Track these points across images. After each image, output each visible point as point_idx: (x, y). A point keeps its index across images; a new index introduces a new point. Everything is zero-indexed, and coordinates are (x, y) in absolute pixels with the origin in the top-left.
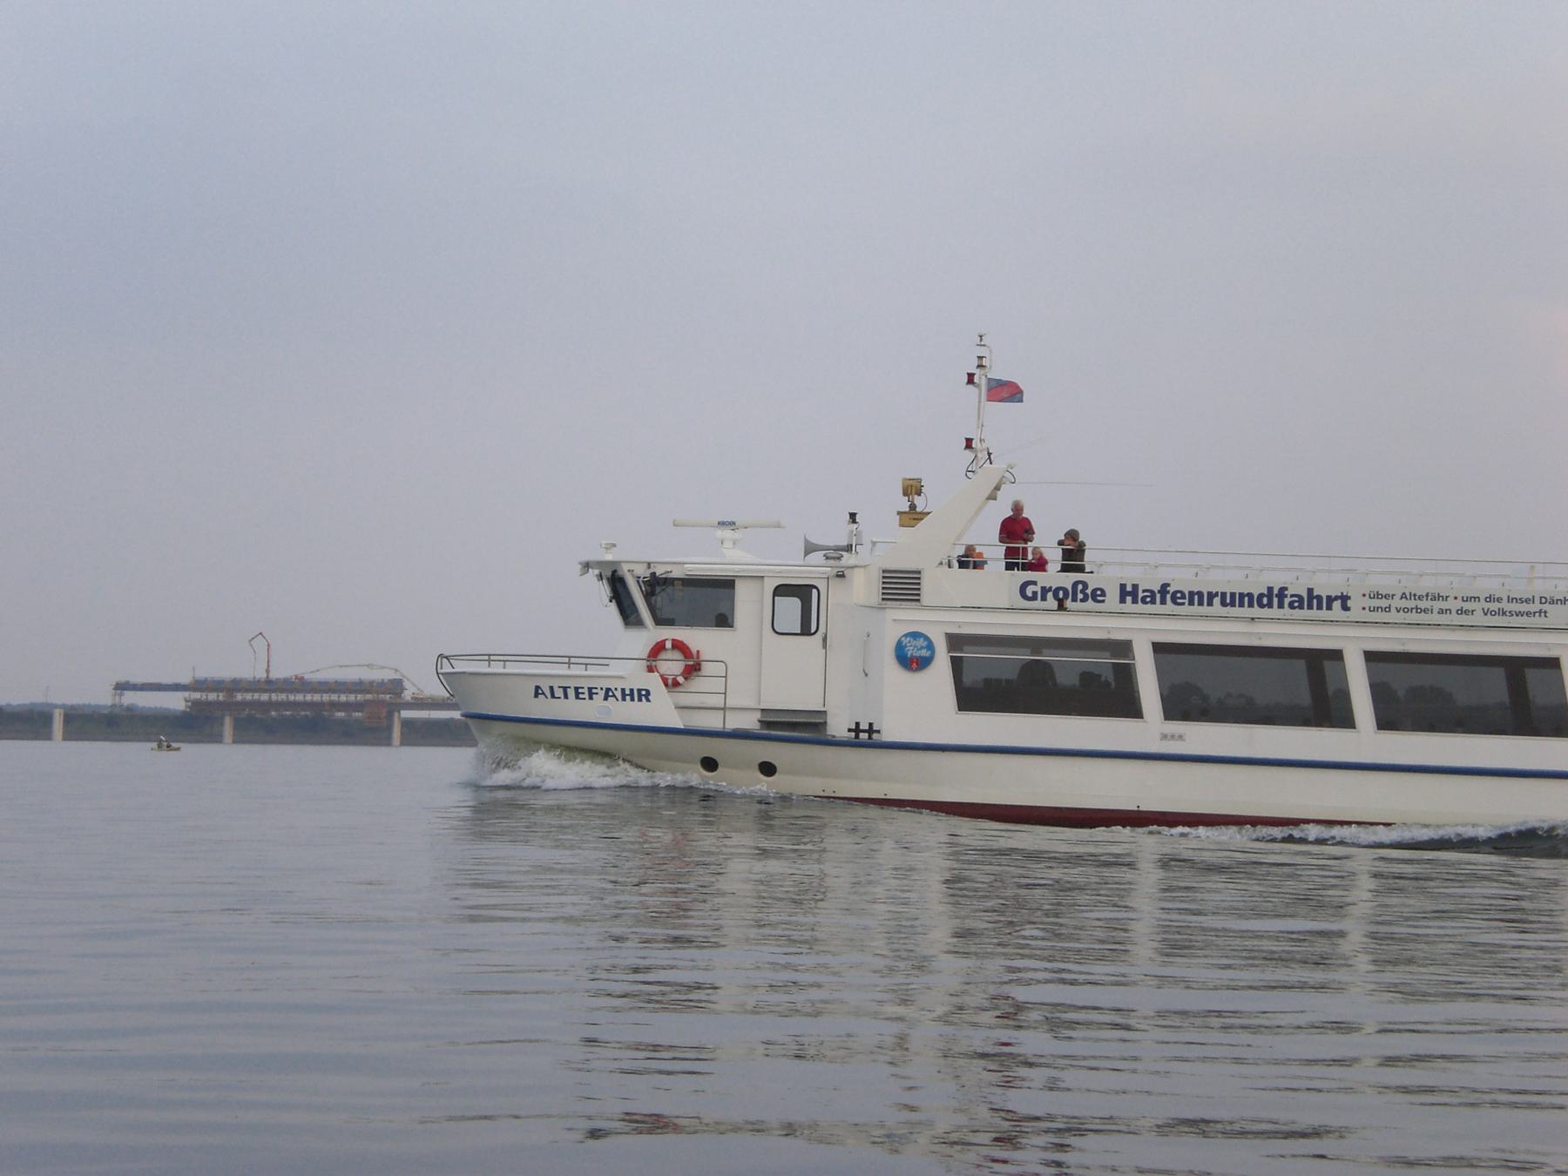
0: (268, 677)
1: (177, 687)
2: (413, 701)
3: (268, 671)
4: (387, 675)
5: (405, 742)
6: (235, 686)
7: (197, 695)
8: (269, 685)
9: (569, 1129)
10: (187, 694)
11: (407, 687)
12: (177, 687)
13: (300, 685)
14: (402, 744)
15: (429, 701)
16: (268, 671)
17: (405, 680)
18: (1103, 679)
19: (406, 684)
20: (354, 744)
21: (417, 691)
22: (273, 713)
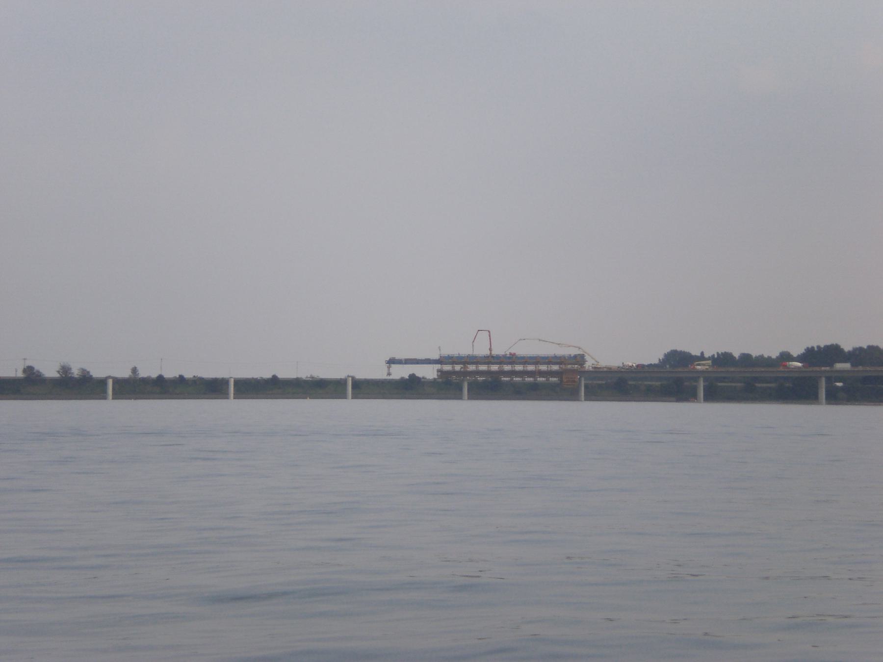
0: (491, 353)
1: (428, 361)
2: (593, 370)
3: (490, 350)
4: (573, 352)
5: (471, 397)
6: (465, 360)
7: (447, 368)
8: (490, 359)
9: (850, 579)
10: (438, 366)
11: (587, 360)
12: (428, 361)
13: (512, 359)
14: (586, 400)
15: (605, 369)
16: (490, 350)
17: (586, 354)
18: (816, 349)
19: (587, 357)
20: (524, 399)
21: (596, 363)
22: (468, 378)
